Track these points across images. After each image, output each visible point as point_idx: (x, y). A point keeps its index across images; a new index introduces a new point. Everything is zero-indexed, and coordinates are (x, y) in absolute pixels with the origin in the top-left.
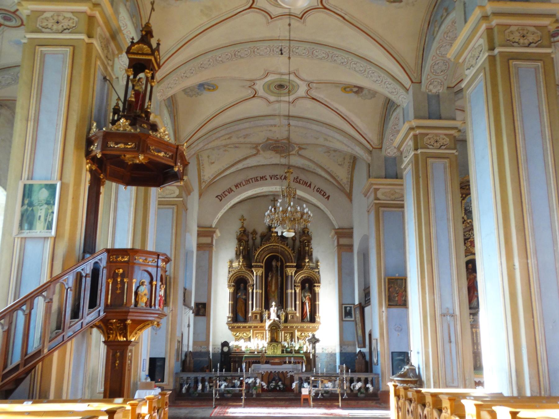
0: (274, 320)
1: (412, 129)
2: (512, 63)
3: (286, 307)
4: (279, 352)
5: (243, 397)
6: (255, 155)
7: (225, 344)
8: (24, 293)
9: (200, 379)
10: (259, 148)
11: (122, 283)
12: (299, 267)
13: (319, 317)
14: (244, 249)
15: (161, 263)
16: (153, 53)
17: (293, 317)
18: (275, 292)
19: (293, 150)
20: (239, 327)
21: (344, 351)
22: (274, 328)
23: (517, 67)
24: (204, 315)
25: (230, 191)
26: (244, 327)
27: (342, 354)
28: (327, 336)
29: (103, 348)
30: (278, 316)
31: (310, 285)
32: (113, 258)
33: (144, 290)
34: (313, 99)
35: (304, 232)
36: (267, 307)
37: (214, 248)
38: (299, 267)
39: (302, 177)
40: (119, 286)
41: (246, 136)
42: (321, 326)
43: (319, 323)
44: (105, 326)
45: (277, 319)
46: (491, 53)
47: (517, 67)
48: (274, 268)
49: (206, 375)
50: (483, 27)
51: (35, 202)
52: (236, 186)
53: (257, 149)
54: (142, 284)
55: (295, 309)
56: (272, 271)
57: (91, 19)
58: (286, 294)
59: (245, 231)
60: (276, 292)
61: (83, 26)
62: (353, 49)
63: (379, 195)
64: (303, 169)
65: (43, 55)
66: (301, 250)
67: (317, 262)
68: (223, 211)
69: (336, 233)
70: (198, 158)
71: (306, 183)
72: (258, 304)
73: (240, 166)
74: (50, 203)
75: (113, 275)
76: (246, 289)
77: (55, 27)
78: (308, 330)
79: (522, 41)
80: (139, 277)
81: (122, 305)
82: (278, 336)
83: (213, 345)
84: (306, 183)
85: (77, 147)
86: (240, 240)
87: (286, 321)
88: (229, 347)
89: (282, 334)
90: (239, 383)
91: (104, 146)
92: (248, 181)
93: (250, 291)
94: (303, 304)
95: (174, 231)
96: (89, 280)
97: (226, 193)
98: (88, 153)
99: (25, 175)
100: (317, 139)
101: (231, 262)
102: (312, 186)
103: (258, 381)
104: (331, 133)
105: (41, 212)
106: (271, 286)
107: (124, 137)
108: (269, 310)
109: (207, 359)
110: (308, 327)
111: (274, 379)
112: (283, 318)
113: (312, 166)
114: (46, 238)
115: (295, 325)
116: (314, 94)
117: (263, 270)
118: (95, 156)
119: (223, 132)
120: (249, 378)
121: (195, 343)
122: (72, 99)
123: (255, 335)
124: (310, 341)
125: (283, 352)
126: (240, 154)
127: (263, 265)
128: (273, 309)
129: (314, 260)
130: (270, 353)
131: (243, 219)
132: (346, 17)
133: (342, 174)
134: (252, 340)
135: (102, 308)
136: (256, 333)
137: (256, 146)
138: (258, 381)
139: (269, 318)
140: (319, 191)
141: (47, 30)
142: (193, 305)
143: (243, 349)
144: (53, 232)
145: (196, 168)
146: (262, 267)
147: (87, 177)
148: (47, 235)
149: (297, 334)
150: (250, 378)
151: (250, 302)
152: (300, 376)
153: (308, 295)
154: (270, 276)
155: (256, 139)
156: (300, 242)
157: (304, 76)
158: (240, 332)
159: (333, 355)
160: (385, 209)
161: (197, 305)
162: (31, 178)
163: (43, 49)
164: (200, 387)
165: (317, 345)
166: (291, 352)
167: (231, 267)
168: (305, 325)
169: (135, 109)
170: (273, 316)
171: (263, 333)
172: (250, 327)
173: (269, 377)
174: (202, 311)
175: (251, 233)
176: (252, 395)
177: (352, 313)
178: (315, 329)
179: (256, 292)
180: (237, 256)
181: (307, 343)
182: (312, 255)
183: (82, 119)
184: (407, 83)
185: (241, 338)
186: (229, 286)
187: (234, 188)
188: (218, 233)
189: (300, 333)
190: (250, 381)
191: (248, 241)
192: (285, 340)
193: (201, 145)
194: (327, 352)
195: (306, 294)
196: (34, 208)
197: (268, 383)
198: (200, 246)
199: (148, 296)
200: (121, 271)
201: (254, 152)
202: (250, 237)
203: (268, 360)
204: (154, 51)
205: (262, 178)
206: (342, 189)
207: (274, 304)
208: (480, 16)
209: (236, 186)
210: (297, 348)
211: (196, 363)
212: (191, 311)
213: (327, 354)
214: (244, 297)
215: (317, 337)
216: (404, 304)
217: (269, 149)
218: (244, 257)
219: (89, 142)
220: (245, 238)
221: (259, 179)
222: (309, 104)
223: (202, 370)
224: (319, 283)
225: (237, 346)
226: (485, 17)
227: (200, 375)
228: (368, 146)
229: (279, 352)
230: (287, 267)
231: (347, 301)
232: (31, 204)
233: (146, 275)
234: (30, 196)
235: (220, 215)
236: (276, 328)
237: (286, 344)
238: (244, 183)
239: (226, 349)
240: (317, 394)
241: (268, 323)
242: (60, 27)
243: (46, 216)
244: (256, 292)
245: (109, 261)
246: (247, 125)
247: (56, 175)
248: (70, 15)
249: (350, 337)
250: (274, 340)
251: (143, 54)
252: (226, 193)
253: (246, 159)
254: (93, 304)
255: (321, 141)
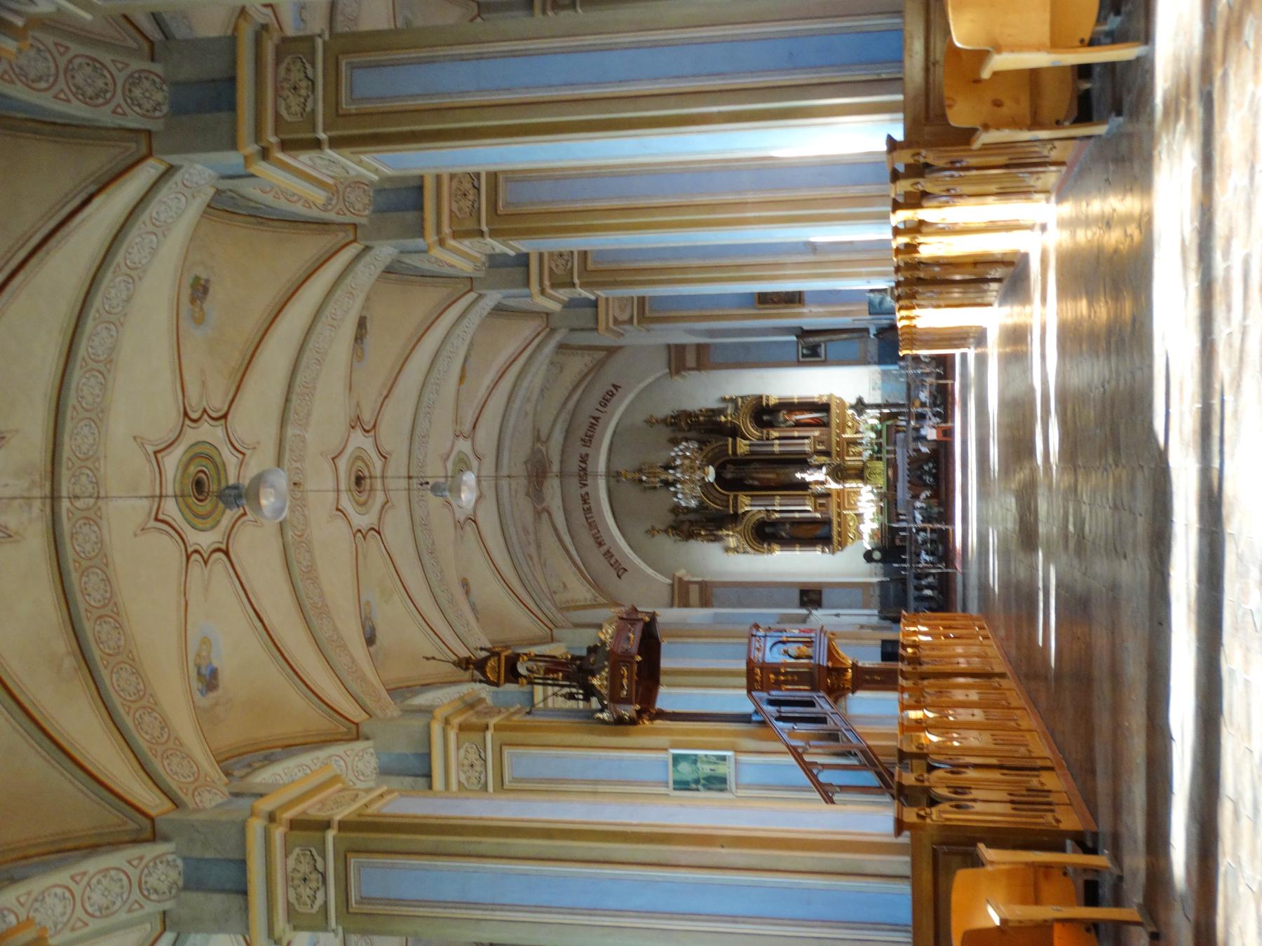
0: (827, 474)
1: (543, 292)
2: (501, 210)
3: (804, 453)
4: (880, 465)
5: (944, 527)
6: (550, 515)
7: (868, 556)
8: (801, 777)
9: (917, 593)
10: (539, 508)
11: (786, 673)
12: (735, 432)
13: (821, 397)
14: (703, 528)
15: (761, 633)
16: (498, 654)
17: (822, 442)
18: (778, 472)
19: (541, 451)
20: (839, 534)
21: (876, 359)
22: (840, 473)
23: (507, 204)
24: (820, 593)
25: (608, 555)
26: (839, 524)
27: (881, 362)
28: (848, 384)
29: (860, 694)
30: (820, 467)
31: (765, 413)
32: (757, 686)
33: (793, 649)
34: (474, 427)
35: (672, 424)
36: (804, 485)
37: (707, 579)
38: (735, 432)
39: (581, 432)
40: (790, 678)
41: (526, 531)
42: (837, 393)
43: (830, 396)
44: (837, 693)
45: (824, 469)
46: (487, 235)
47: (507, 204)
48: (738, 475)
49: (912, 583)
50: (452, 243)
51: (695, 776)
52: (600, 544)
53: (541, 511)
54: (786, 652)
55: (808, 438)
56: (741, 479)
57: (463, 728)
58: (782, 453)
59: (673, 528)
60: (779, 471)
61: (476, 737)
62: (421, 378)
63: (626, 317)
64: (567, 431)
65: (363, 900)
66: (708, 428)
67: (724, 400)
68: (643, 565)
69: (678, 372)
70: (568, 609)
71: (592, 426)
72: (801, 502)
73: (567, 539)
74: (694, 760)
75: (778, 685)
76: (775, 523)
77: (478, 768)
78: (843, 416)
79: (471, 197)
80: (774, 656)
81: (810, 674)
82: (854, 468)
83: (871, 576)
84: (592, 426)
85: (626, 734)
86: (690, 536)
87: (827, 453)
88: (873, 549)
89: (851, 461)
90: (922, 534)
91: (627, 701)
92: (590, 524)
93: (777, 515)
94: (799, 424)
95: (690, 640)
96: (783, 709)
97: (612, 561)
98: (633, 722)
99: (662, 790)
100: (526, 414)
101: (727, 549)
102: (597, 414)
103: (918, 504)
104: (521, 393)
105: (706, 769)
106: (769, 480)
107: (614, 679)
108: (810, 483)
109: (892, 586)
110: (838, 416)
111: (920, 478)
112: (823, 459)
113: (565, 416)
114: (736, 762)
115: (834, 439)
116: (467, 427)
117: (740, 494)
118: (637, 712)
119: (526, 569)
120: (914, 518)
121: (866, 606)
122: (569, 743)
123: (853, 506)
124: (860, 412)
125: (879, 459)
126: (550, 541)
127: (732, 494)
128: (810, 477)
129: (722, 405)
130: (881, 482)
131: (651, 532)
132: (385, 393)
133: (577, 365)
134: (861, 511)
135: (814, 695)
136: (849, 503)
137: (538, 514)
138: (918, 504)
139: (822, 483)
140: (605, 402)
141: (483, 777)
142: (804, 611)
143: (876, 526)
144: (728, 753)
145: (579, 613)
146: (736, 497)
147: (659, 723)
148: (732, 761)
149: (849, 435)
150: (915, 519)
151: (797, 515)
152: (911, 439)
153: (782, 415)
154: (751, 482)
155: (529, 516)
156: (690, 430)
157: (449, 444)
158: (847, 531)
159: (884, 373)
160: (647, 308)
161: (803, 604)
162: (666, 784)
163: (506, 779)
164: (928, 592)
165: (866, 401)
166: (880, 445)
167: (736, 550)
168: (835, 420)
169: (575, 672)
170: (820, 475)
171: (849, 493)
172: (839, 515)
173: (916, 484)
174: (814, 597)
175: (677, 515)
176: (940, 513)
177: (812, 348)
178: (842, 404)
179: (780, 507)
180: (717, 539)
181: (865, 417)
182: (712, 411)
183: (591, 732)
184: (472, 296)
185: (857, 529)
186: (770, 551)
187: (604, 548)
188: (680, 573)
189: (848, 430)
190: (919, 517)
191: (691, 522)
192: (860, 454)
193: (548, 603)
194: (879, 382)
195: (781, 419)
196: (702, 776)
197: (926, 486)
198: (705, 602)
199: (801, 645)
200: (772, 676)
201: (545, 516)
202: (682, 517)
203: (892, 485)
204: (494, 654)
205: (585, 501)
206: (599, 366)
207: (799, 475)
208: (439, 248)
209: (600, 544)
210: (873, 435)
211: (894, 600)
212: (814, 612)
213: (883, 381)
214: (788, 526)
215: (853, 402)
216: (800, 293)
217: (541, 491)
218: (720, 528)
219: (620, 721)
220: (685, 527)
221: (586, 506)
222: (481, 433)
223: (905, 591)
224: (761, 397)
225: (871, 537)
226: (441, 242)
227: (912, 593)
228: (543, 334)
229: (880, 465)
230: (734, 452)
231: (792, 354)
232: (697, 781)
233: (775, 649)
234: (687, 783)
235: (650, 571)
236: (841, 471)
237: (867, 454)
238: (595, 531)
239: (877, 555)
240: (936, 415)
241: (833, 485)
242: (478, 763)
243: (710, 763)
244: (780, 507)
245: (762, 690)
246: (512, 530)
247: (661, 755)
248: (462, 752)
249: (855, 347)
250: (860, 474)
251: (499, 666)
252: (612, 561)
253: (556, 529)
254: (811, 704)
255: (529, 407)
